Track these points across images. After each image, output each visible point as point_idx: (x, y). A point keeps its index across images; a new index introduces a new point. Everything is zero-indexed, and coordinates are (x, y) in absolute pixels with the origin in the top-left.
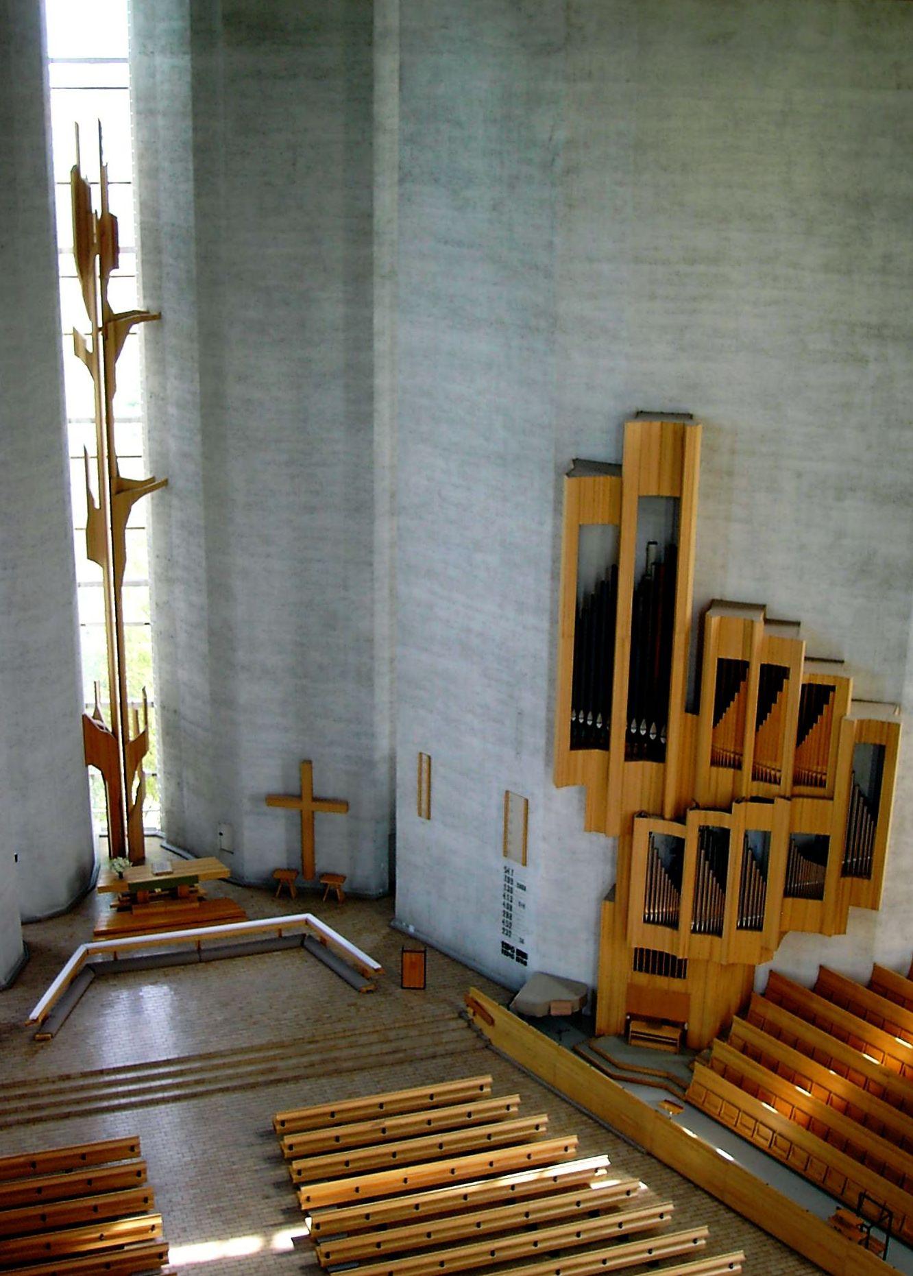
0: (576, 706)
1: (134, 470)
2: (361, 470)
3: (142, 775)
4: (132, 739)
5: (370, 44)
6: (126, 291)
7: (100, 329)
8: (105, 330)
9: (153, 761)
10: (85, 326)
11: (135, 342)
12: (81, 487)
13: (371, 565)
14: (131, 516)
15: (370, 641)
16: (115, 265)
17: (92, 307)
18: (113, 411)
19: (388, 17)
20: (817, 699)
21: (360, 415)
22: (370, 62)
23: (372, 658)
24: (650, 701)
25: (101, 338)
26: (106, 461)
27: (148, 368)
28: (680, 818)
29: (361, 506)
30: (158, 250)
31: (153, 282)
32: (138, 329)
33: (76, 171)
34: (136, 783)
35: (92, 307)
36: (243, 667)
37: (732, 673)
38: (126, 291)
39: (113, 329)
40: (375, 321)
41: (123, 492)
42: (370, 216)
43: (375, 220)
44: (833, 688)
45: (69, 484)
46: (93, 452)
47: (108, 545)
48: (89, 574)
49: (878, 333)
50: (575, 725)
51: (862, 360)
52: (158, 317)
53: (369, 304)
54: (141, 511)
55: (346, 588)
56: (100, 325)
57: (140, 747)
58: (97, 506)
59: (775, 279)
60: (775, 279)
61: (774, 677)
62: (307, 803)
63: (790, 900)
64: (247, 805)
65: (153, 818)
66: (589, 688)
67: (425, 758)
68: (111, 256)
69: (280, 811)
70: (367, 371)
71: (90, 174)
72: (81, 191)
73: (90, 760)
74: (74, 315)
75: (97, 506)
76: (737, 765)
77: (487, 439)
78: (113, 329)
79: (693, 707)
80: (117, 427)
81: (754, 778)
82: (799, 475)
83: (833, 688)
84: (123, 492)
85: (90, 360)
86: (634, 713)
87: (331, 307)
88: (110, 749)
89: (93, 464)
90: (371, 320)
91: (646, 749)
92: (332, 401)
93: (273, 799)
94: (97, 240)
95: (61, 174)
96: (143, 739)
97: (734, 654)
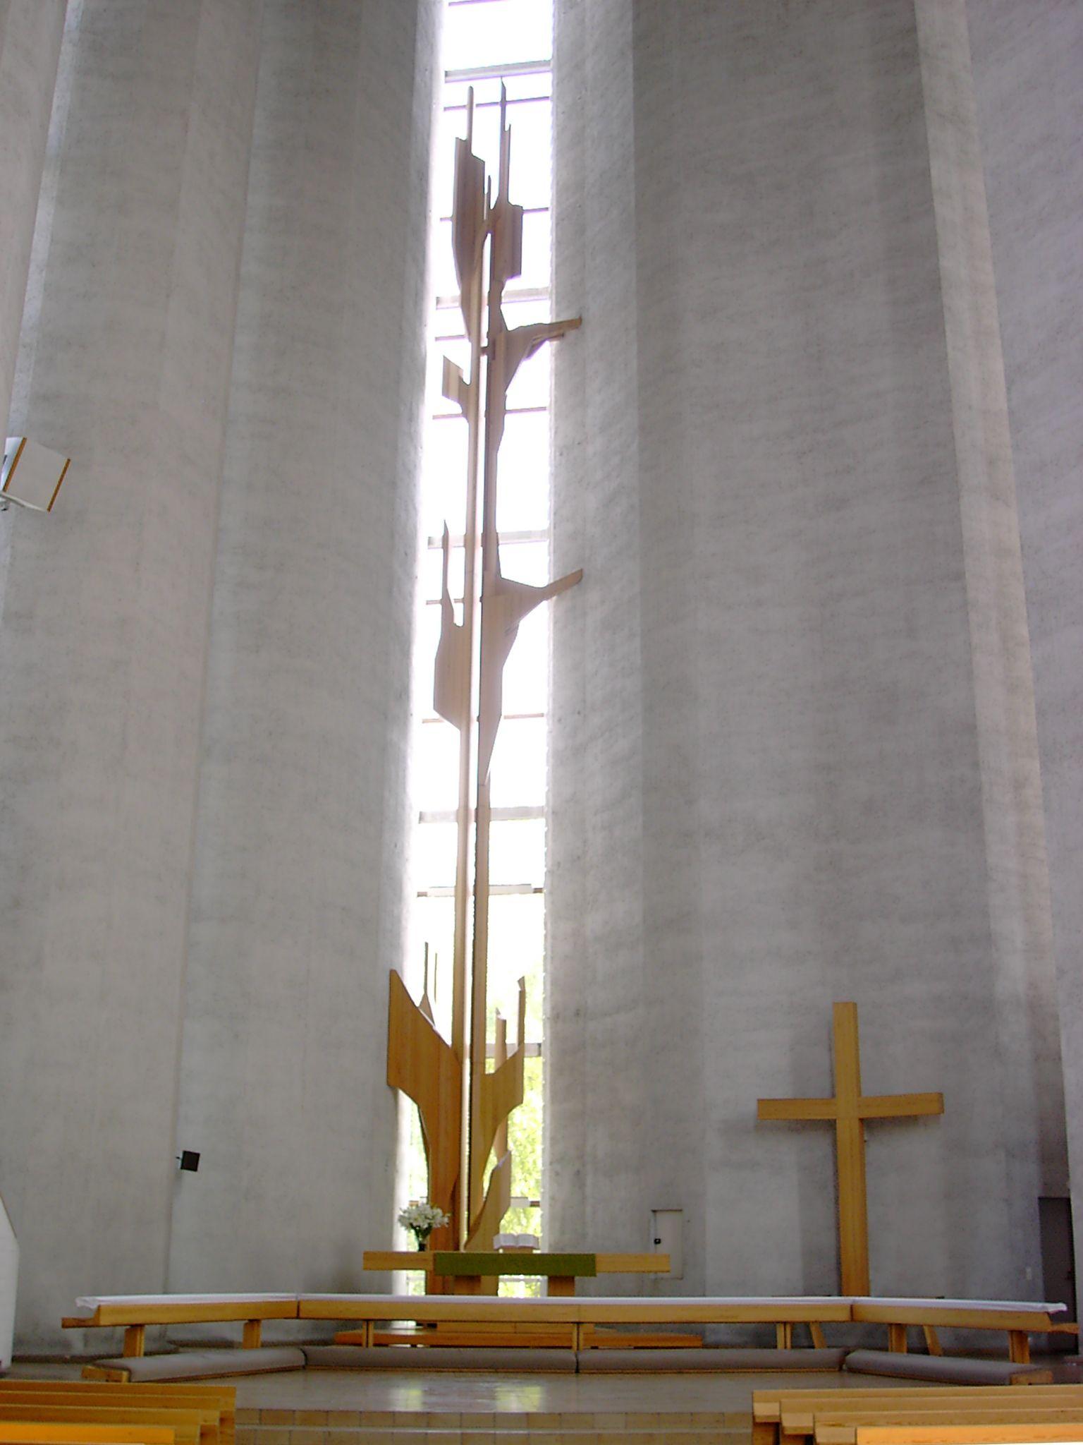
3: (505, 1154)
6: (529, 300)
7: (484, 350)
9: (529, 1125)
10: (462, 354)
11: (535, 377)
12: (434, 584)
13: (959, 576)
14: (525, 324)
15: (970, 728)
16: (515, 270)
17: (474, 321)
18: (491, 477)
19: (945, 23)
23: (976, 765)
25: (484, 360)
26: (471, 899)
27: (555, 650)
32: (547, 351)
33: (464, 148)
34: (493, 1162)
35: (474, 321)
38: (529, 300)
39: (504, 350)
40: (934, 172)
41: (504, 602)
42: (913, 29)
43: (921, 35)
45: (424, 360)
46: (458, 532)
47: (467, 690)
52: (576, 323)
54: (536, 631)
56: (485, 343)
57: (503, 1091)
58: (459, 620)
68: (508, 264)
70: (929, 248)
71: (486, 150)
72: (469, 170)
75: (459, 620)
78: (504, 350)
80: (494, 903)
84: (504, 602)
85: (462, 392)
88: (446, 1077)
89: (458, 556)
90: (925, 173)
93: (778, 1118)
94: (487, 228)
95: (444, 134)
96: (512, 1067)
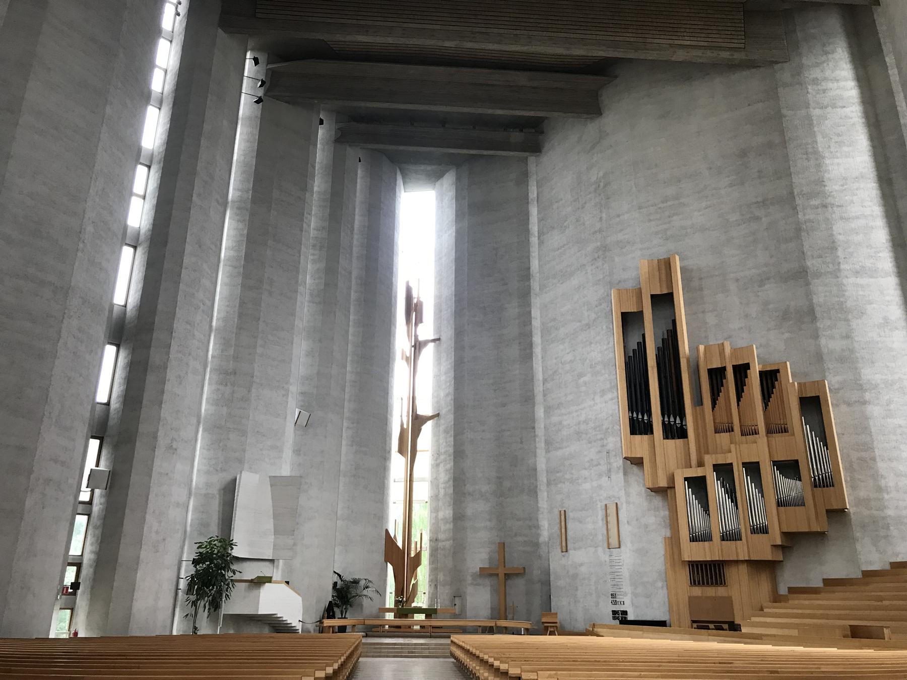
0: (631, 408)
1: (425, 409)
2: (528, 380)
4: (412, 555)
5: (528, 203)
6: (426, 331)
8: (415, 346)
13: (534, 428)
20: (770, 378)
21: (527, 354)
22: (527, 209)
24: (673, 404)
28: (701, 464)
29: (528, 399)
30: (441, 311)
31: (438, 329)
36: (469, 494)
37: (717, 375)
38: (426, 331)
39: (418, 346)
44: (778, 371)
47: (409, 448)
48: (397, 464)
49: (764, 203)
50: (631, 420)
51: (757, 219)
52: (439, 339)
53: (529, 305)
54: (427, 429)
55: (522, 443)
59: (707, 197)
60: (707, 197)
61: (742, 371)
62: (501, 572)
63: (780, 508)
64: (469, 579)
65: (421, 601)
66: (637, 398)
67: (563, 512)
68: (419, 320)
69: (487, 582)
73: (388, 559)
74: (401, 342)
76: (731, 430)
77: (580, 321)
78: (418, 346)
79: (698, 401)
81: (742, 435)
82: (737, 280)
83: (778, 371)
84: (418, 421)
86: (665, 410)
87: (512, 309)
88: (400, 558)
91: (675, 432)
92: (514, 351)
94: (413, 309)
96: (418, 555)
97: (716, 364)
